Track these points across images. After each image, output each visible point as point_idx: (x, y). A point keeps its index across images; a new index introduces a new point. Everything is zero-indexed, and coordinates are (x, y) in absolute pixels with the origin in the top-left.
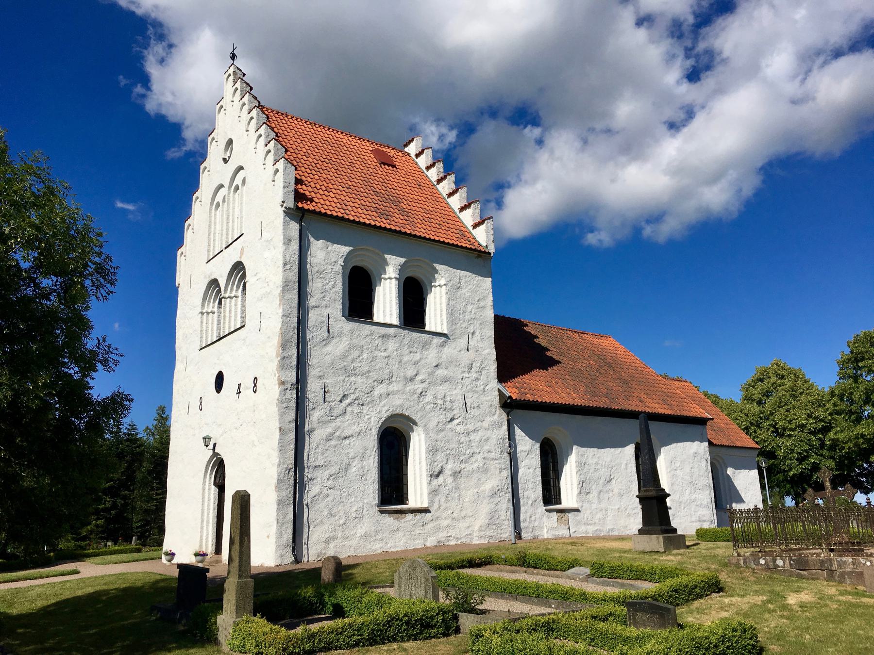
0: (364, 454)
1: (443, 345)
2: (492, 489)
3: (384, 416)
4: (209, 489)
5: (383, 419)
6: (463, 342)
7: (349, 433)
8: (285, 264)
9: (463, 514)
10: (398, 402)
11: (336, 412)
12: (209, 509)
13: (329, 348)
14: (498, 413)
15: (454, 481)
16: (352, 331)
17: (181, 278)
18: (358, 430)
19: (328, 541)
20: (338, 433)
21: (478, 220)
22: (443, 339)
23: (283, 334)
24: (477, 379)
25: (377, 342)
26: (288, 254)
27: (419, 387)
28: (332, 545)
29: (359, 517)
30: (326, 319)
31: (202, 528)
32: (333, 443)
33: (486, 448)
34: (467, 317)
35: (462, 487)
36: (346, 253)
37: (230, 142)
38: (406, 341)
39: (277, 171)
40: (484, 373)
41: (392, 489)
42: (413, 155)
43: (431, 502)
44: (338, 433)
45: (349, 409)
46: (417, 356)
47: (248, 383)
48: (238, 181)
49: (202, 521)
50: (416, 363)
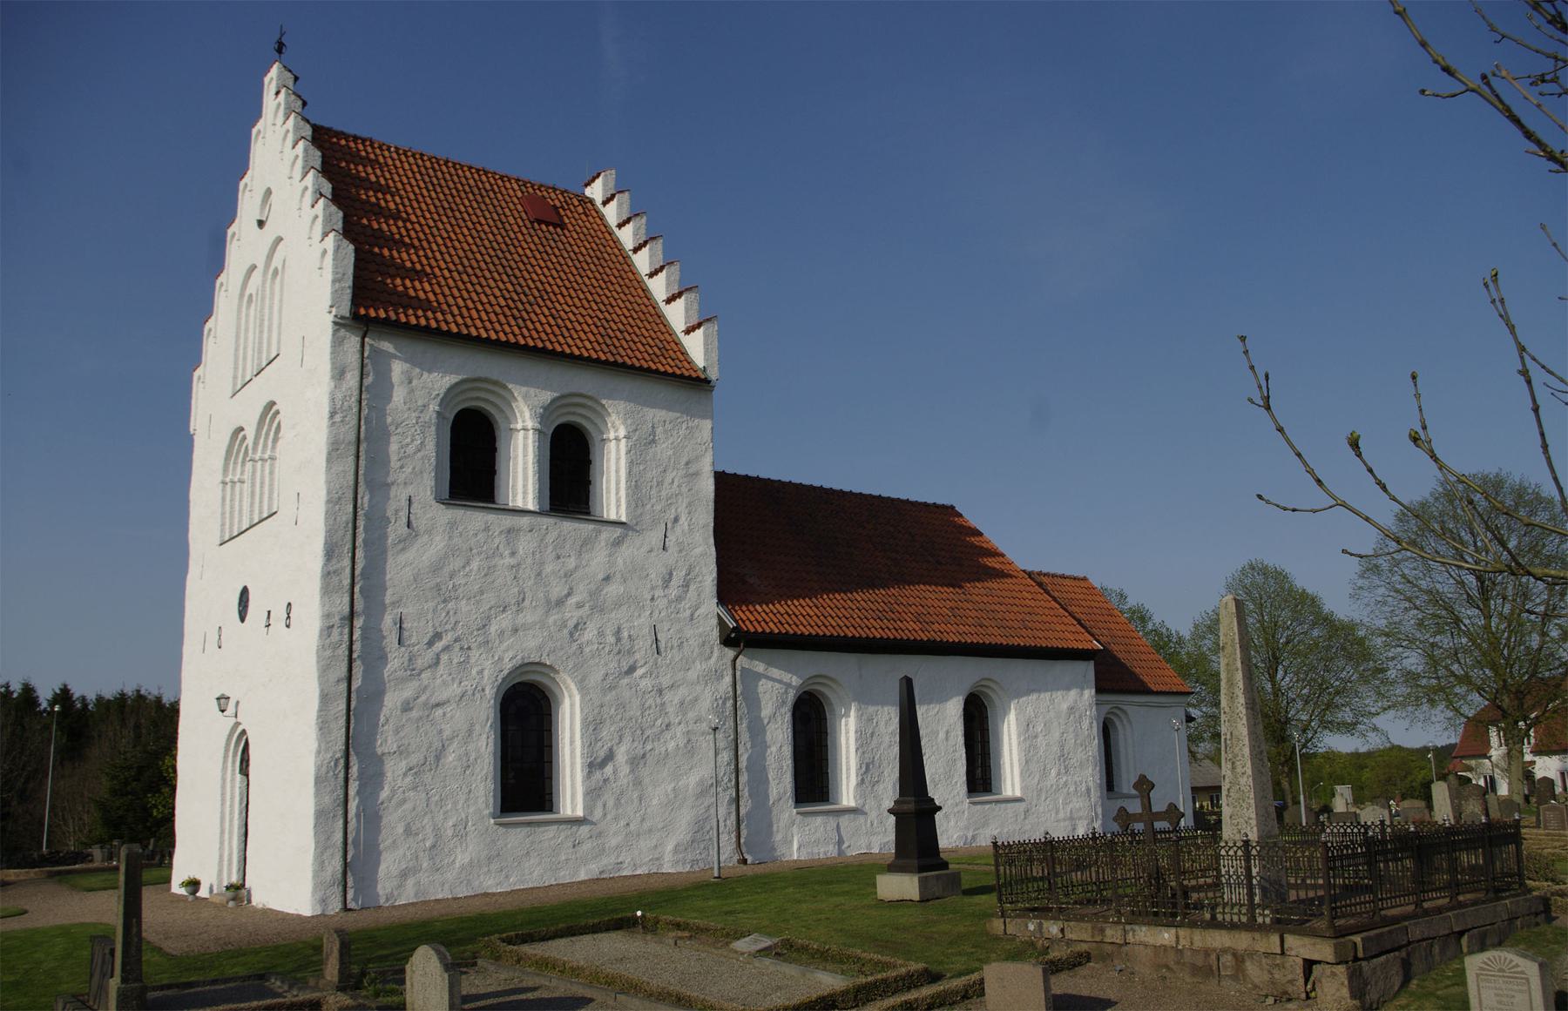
0: (470, 732)
1: (618, 543)
2: (701, 782)
3: (508, 666)
4: (233, 780)
5: (506, 672)
6: (655, 537)
7: (444, 696)
8: (332, 414)
9: (646, 825)
10: (531, 643)
11: (420, 663)
12: (231, 813)
13: (410, 554)
14: (716, 654)
15: (632, 771)
16: (452, 525)
17: (199, 422)
18: (459, 691)
19: (404, 875)
20: (423, 698)
21: (695, 321)
22: (619, 531)
23: (330, 533)
24: (679, 599)
25: (497, 541)
26: (339, 396)
27: (571, 614)
28: (410, 882)
29: (460, 833)
30: (405, 504)
31: (222, 843)
32: (414, 714)
33: (691, 715)
34: (663, 493)
35: (647, 780)
36: (443, 391)
37: (269, 192)
38: (550, 538)
39: (325, 251)
40: (692, 587)
41: (525, 782)
42: (599, 200)
43: (589, 807)
44: (423, 698)
45: (444, 657)
46: (572, 563)
47: (279, 614)
48: (276, 262)
49: (222, 832)
50: (568, 575)
